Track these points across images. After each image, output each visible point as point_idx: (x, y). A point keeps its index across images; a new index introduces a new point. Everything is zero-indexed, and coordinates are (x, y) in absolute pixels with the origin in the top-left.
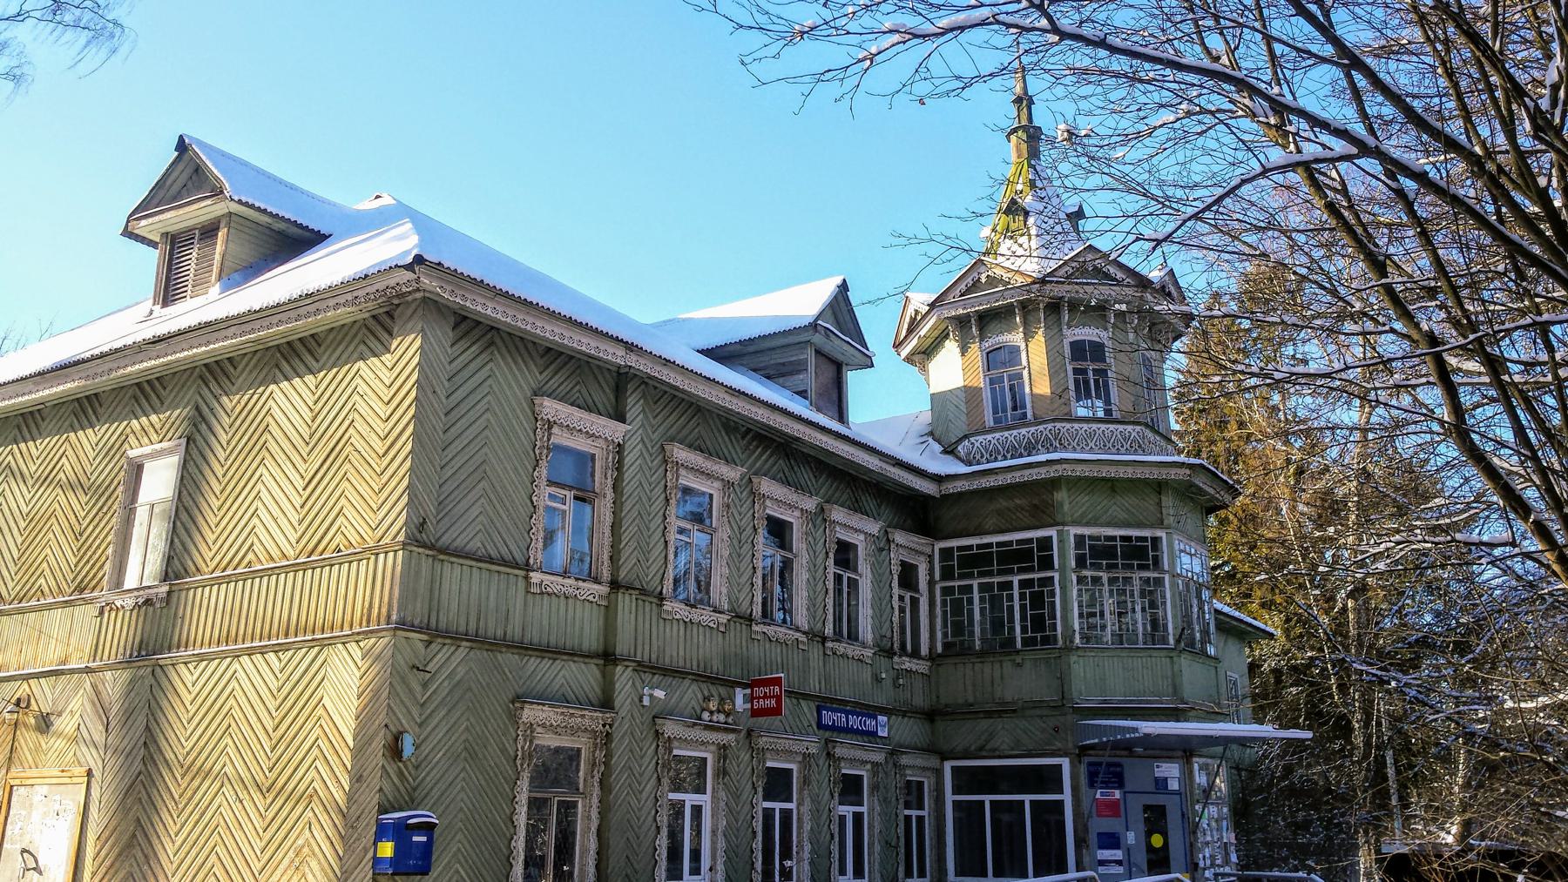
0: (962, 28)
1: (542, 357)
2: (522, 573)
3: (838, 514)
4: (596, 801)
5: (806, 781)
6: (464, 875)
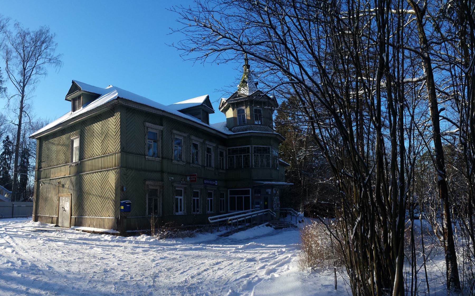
0: (225, 49)
3: (207, 142)
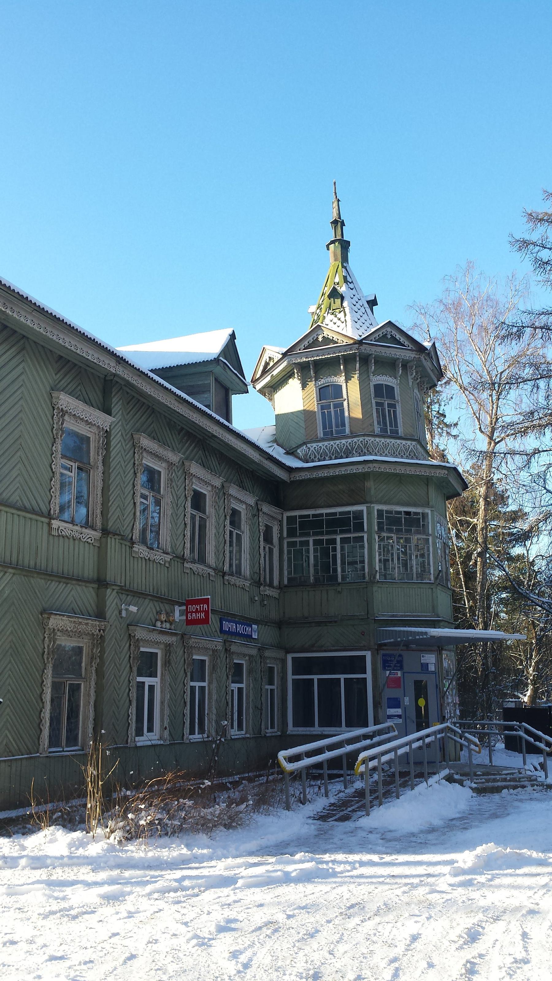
1: (56, 362)
2: (46, 520)
4: (94, 683)
5: (214, 668)
6: (12, 740)
